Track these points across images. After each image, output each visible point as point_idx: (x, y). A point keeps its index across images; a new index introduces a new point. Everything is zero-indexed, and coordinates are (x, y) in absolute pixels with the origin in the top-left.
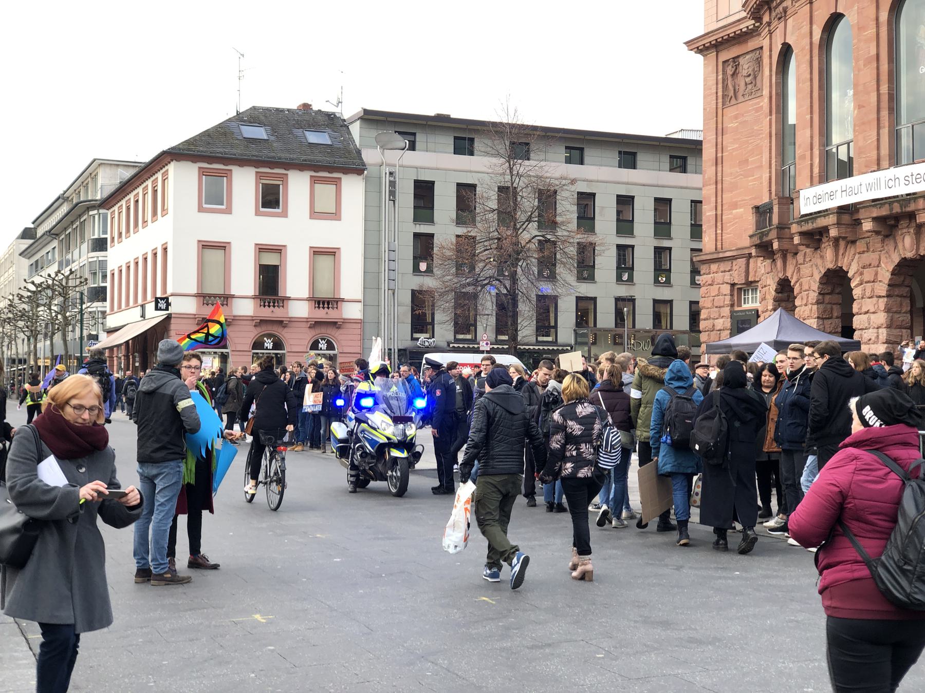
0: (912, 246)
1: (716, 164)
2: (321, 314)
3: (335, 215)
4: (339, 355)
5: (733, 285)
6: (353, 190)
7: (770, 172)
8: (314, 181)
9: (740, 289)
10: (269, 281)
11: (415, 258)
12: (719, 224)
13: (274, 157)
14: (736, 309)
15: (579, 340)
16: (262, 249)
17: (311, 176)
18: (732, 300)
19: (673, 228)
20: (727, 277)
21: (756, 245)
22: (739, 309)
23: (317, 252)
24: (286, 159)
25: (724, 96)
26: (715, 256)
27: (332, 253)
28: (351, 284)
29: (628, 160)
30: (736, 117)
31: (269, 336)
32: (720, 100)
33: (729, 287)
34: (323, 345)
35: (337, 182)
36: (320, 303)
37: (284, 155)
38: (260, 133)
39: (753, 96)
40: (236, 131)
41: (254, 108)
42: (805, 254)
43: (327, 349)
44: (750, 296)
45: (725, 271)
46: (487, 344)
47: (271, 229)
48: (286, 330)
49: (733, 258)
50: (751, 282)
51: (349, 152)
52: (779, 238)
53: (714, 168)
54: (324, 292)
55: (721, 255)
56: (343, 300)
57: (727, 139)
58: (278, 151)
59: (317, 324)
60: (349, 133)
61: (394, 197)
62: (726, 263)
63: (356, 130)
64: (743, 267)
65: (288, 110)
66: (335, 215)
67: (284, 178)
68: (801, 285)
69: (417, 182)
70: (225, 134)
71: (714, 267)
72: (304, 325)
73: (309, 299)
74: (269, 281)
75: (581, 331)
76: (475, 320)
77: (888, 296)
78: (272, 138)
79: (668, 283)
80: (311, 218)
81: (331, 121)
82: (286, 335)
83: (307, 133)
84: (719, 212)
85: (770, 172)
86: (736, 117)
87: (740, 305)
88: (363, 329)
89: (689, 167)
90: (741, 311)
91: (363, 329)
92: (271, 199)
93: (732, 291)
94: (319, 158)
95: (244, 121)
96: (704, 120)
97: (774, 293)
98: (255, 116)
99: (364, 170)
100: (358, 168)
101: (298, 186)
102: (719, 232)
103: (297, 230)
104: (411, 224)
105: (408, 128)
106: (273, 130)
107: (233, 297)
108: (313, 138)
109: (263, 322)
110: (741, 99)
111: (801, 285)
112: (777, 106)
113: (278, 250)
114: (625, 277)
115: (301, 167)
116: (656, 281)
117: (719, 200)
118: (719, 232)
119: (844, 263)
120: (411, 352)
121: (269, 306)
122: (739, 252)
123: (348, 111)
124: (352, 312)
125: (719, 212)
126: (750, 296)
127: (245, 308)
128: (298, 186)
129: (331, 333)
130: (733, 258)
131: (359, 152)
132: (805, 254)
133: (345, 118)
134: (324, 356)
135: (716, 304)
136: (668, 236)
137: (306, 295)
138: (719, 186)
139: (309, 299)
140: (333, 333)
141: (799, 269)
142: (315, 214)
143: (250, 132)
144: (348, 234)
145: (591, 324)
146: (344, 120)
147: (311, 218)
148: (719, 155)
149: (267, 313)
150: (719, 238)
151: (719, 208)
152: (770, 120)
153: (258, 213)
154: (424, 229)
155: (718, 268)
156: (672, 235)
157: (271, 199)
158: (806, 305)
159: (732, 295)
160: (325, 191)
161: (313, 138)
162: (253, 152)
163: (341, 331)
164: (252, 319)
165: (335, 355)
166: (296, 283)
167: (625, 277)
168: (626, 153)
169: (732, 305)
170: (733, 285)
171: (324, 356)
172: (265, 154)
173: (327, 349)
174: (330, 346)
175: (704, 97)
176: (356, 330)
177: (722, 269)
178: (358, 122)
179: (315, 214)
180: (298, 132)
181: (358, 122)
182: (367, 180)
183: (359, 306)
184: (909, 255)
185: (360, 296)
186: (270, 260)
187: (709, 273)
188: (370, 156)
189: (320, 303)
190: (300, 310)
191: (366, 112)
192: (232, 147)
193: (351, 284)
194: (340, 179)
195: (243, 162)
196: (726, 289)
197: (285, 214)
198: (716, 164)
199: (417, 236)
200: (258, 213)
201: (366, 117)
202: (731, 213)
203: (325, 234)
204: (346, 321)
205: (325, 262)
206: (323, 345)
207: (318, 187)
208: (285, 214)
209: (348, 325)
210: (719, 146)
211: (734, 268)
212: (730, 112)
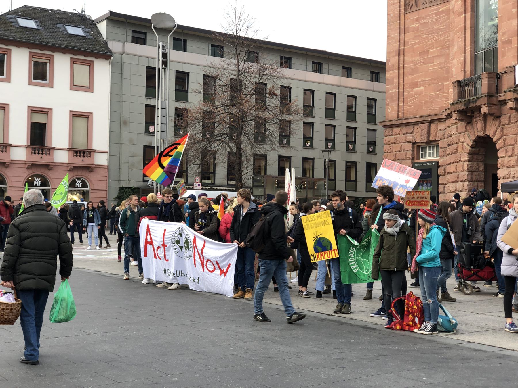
0: (482, 128)
1: (399, 55)
2: (78, 161)
3: (89, 88)
4: (91, 191)
5: (414, 144)
6: (102, 70)
7: (465, 56)
8: (73, 62)
9: (418, 147)
10: (38, 134)
11: (146, 123)
12: (401, 99)
13: (43, 42)
14: (416, 161)
15: (256, 184)
16: (33, 111)
17: (71, 58)
18: (413, 154)
19: (315, 111)
20: (409, 138)
21: (458, 111)
22: (418, 161)
23: (75, 115)
24: (53, 43)
25: (406, 5)
26: (399, 122)
27: (87, 116)
28: (100, 139)
29: (286, 62)
30: (417, 20)
31: (38, 176)
32: (403, 8)
33: (410, 145)
34: (79, 184)
35: (91, 65)
36: (77, 152)
37: (52, 41)
38: (31, 24)
39: (432, 4)
40: (13, 21)
41: (25, 7)
42: (510, 116)
43: (82, 187)
44: (427, 152)
45: (407, 133)
46: (199, 185)
47: (39, 96)
48: (51, 172)
49: (417, 123)
50: (431, 141)
51: (99, 43)
52: (489, 104)
53: (397, 57)
54: (80, 145)
55: (405, 121)
56: (95, 151)
57: (409, 36)
58: (46, 37)
59: (74, 168)
60: (97, 29)
61: (166, 66)
62: (408, 127)
63: (103, 27)
64: (426, 130)
65: (51, 10)
66: (89, 88)
67: (51, 59)
68: (504, 141)
69: (148, 68)
70: (5, 23)
71: (396, 130)
72: (65, 168)
73: (69, 150)
74: (38, 134)
75: (256, 177)
76: (187, 169)
77: (469, 161)
78: (41, 28)
79: (311, 147)
80: (71, 89)
81: (80, 19)
82: (51, 176)
83: (67, 27)
84: (401, 90)
85: (465, 56)
86: (417, 20)
87: (418, 158)
88: (108, 173)
89: (324, 70)
90: (420, 163)
91: (108, 173)
92: (40, 73)
93: (413, 147)
94: (75, 44)
95: (19, 15)
96: (388, 23)
97: (469, 148)
98: (26, 12)
99: (111, 56)
100: (105, 54)
101: (61, 65)
102: (401, 104)
103: (60, 97)
104: (144, 98)
105: (138, 29)
106: (41, 22)
107: (11, 145)
108: (72, 30)
109: (34, 165)
110: (421, 6)
111: (504, 141)
112: (472, 7)
113: (46, 112)
114: (285, 141)
115: (64, 50)
116: (304, 145)
117: (401, 81)
118: (401, 104)
119: (490, 132)
120: (143, 190)
121: (39, 154)
122: (422, 119)
123: (95, 12)
124: (102, 160)
125: (401, 90)
126: (427, 152)
127: (20, 154)
128: (61, 65)
129: (85, 175)
130: (417, 123)
131: (106, 43)
132: (510, 116)
133: (93, 19)
134: (79, 192)
135: (398, 158)
136: (312, 116)
137: (67, 147)
138: (401, 71)
139: (69, 150)
140: (87, 175)
141: (502, 129)
142: (74, 87)
143: (24, 23)
144: (98, 102)
145: (263, 173)
146: (93, 21)
147: (71, 89)
148: (402, 48)
149: (37, 158)
150: (401, 109)
151: (401, 87)
152: (465, 17)
153: (30, 83)
154: (150, 102)
155: (401, 131)
156: (314, 115)
157: (40, 73)
158: (510, 156)
159: (413, 151)
160: (82, 70)
161: (72, 30)
162: (28, 36)
163: (92, 174)
164: (25, 163)
165: (88, 191)
166: (59, 136)
167: (285, 141)
168: (286, 58)
169: (413, 159)
170: (414, 144)
171: (79, 192)
172: (37, 38)
173: (82, 187)
174: (84, 185)
175: (389, 6)
176: (104, 173)
177: (404, 132)
178: (105, 22)
179: (74, 87)
180: (60, 26)
181: (105, 22)
182: (112, 64)
183: (106, 156)
184: (481, 134)
185: (106, 149)
186: (39, 119)
187: (392, 135)
188: (115, 46)
189: (77, 152)
190: (62, 157)
191: (112, 13)
192: (11, 32)
193: (100, 139)
194: (93, 61)
195: (20, 44)
196: (409, 146)
197: (51, 85)
198: (399, 55)
199: (147, 106)
200: (30, 83)
201: (113, 18)
202: (412, 91)
203: (81, 102)
204: (97, 167)
205: (81, 123)
206: (79, 184)
207: (76, 66)
208: (51, 85)
209: (97, 170)
210: (402, 42)
211: (416, 131)
212: (412, 16)
